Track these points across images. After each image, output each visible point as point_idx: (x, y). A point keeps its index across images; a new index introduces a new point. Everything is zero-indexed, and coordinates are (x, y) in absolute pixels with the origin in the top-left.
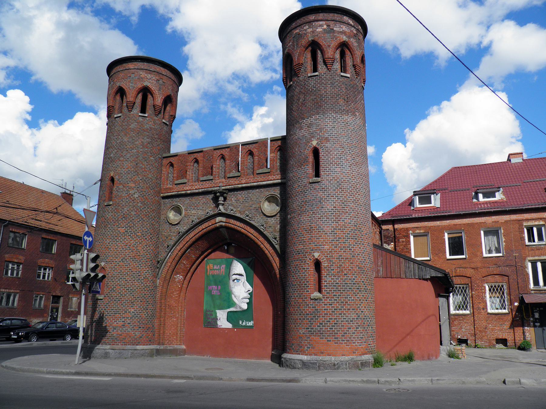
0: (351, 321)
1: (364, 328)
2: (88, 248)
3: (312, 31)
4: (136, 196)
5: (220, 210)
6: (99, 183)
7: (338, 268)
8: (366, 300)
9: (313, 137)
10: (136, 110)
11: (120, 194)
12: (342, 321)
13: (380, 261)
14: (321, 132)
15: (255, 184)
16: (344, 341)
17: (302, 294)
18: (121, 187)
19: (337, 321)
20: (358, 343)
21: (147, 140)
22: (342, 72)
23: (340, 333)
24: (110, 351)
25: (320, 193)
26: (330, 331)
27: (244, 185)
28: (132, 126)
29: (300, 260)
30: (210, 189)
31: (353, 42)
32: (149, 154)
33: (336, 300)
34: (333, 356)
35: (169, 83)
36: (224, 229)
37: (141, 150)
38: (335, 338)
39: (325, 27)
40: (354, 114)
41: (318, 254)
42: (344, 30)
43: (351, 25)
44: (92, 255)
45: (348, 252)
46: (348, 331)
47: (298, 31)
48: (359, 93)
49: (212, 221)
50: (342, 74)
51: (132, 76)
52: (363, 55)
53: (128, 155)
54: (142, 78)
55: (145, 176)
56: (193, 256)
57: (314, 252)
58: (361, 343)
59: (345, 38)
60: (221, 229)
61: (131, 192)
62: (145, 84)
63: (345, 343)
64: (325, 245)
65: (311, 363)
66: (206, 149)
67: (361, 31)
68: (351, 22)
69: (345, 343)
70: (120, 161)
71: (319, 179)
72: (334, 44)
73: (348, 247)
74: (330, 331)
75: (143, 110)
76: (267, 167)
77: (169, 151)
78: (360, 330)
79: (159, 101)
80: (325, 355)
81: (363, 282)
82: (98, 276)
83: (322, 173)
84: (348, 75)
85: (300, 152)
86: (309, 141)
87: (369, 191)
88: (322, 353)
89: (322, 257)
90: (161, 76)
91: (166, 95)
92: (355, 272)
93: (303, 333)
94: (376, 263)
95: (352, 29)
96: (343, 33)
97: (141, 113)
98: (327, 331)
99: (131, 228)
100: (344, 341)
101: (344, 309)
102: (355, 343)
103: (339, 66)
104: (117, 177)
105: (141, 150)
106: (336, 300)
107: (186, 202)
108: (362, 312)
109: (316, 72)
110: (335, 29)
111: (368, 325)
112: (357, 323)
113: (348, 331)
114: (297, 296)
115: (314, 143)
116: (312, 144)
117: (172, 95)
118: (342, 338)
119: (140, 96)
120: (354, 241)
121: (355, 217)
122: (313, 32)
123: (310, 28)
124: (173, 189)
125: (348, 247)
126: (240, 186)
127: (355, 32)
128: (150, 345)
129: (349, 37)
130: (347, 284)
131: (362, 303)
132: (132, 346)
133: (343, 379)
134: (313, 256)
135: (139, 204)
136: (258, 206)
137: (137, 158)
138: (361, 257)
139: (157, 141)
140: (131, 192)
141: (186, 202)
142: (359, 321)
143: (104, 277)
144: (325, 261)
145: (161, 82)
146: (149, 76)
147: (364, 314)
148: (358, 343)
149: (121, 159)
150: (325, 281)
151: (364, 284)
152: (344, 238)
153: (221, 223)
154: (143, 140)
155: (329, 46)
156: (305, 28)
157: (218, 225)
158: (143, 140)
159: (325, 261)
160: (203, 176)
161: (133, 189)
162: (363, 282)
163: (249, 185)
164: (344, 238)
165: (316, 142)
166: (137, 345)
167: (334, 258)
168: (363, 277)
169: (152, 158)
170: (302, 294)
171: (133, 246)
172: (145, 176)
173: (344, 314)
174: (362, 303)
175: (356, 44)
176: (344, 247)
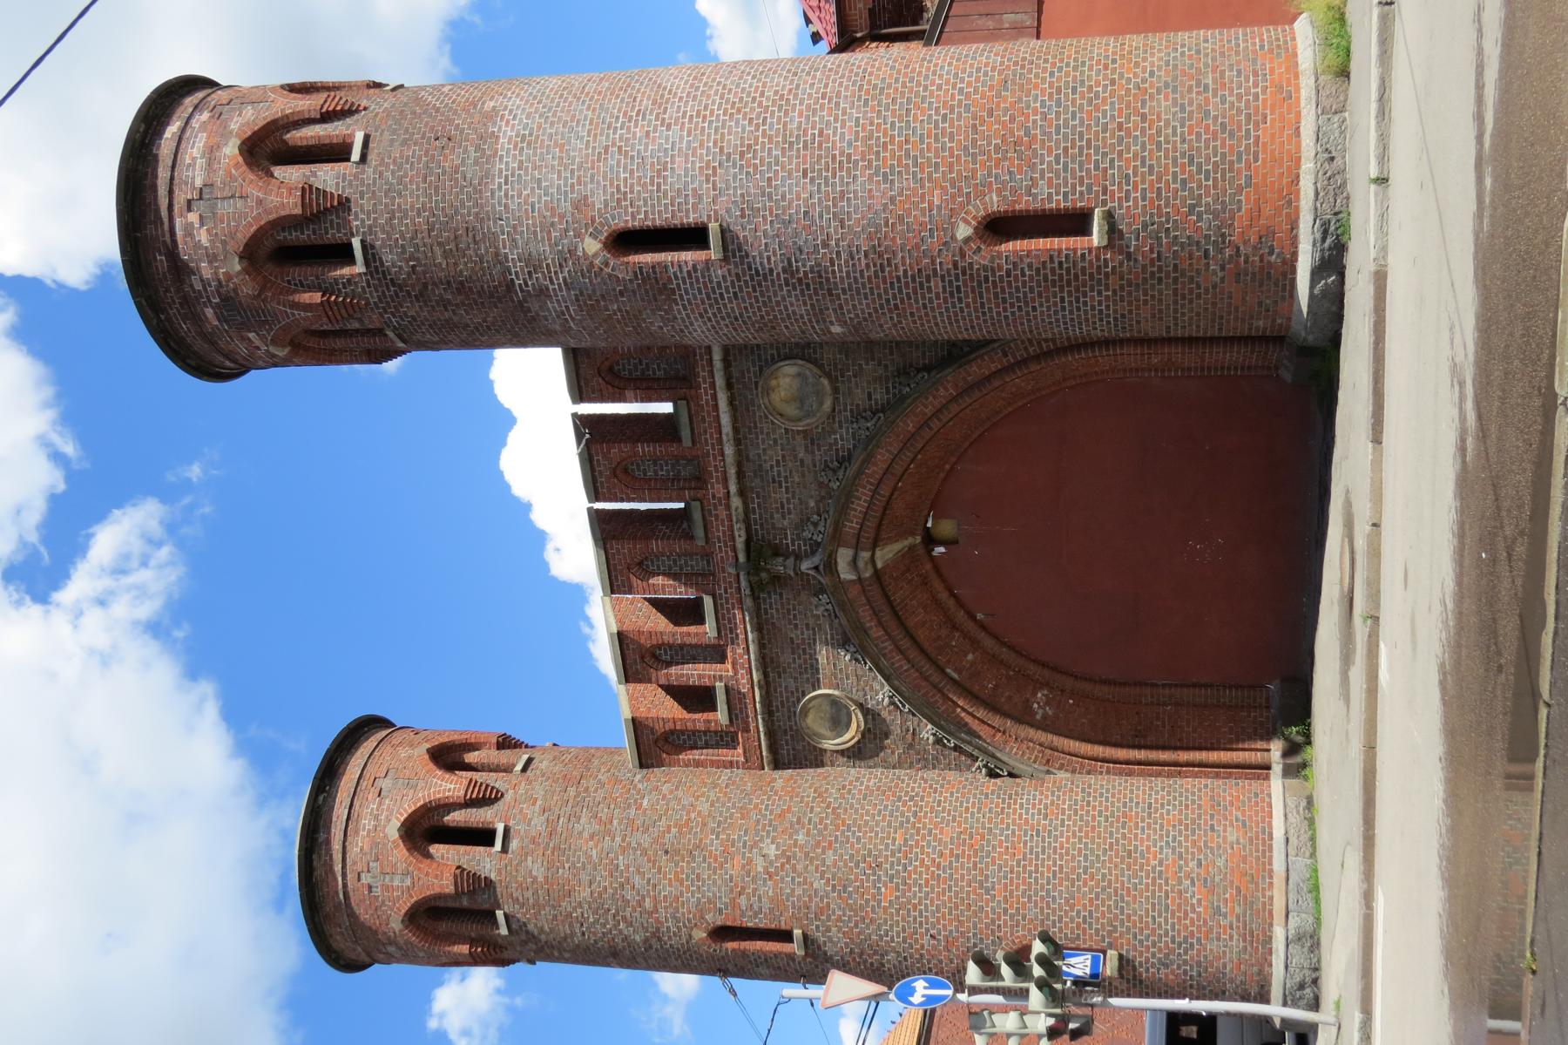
0: (1183, 109)
1: (1206, 65)
2: (950, 992)
3: (210, 262)
4: (772, 851)
5: (816, 568)
6: (733, 980)
7: (1005, 158)
8: (1114, 61)
10: (483, 860)
11: (766, 905)
12: (1183, 141)
13: (981, 22)
14: (553, 224)
16: (1248, 131)
17: (1091, 275)
18: (743, 901)
19: (1183, 155)
20: (1256, 85)
21: (583, 820)
22: (348, 160)
23: (1223, 145)
24: (1293, 923)
26: (1215, 179)
27: (733, 488)
28: (539, 872)
29: (980, 285)
31: (244, 121)
32: (633, 812)
33: (1112, 161)
34: (1298, 166)
35: (386, 757)
36: (878, 553)
37: (618, 839)
38: (1239, 161)
39: (193, 217)
40: (491, 116)
41: (962, 225)
42: (200, 154)
43: (183, 130)
44: (973, 974)
45: (951, 126)
46: (1216, 118)
47: (209, 312)
48: (418, 100)
50: (356, 156)
51: (366, 879)
52: (282, 87)
54: (375, 844)
55: (704, 825)
56: (970, 657)
58: (1256, 74)
59: (231, 149)
60: (879, 565)
61: (760, 865)
62: (393, 830)
63: (1257, 128)
64: (931, 203)
65: (1324, 239)
66: (612, 620)
67: (200, 95)
68: (172, 130)
69: (1257, 128)
71: (713, 227)
72: (251, 184)
73: (936, 127)
74: (1215, 179)
75: (483, 837)
76: (682, 515)
77: (618, 751)
78: (1215, 81)
79: (450, 786)
80: (1298, 191)
81: (1052, 74)
82: (1040, 978)
83: (691, 219)
85: (621, 293)
87: (750, 62)
88: (1290, 202)
90: (364, 784)
91: (431, 765)
92: (1020, 99)
94: (992, 36)
95: (195, 123)
96: (211, 152)
97: (491, 844)
98: (1215, 187)
100: (1248, 131)
102: (1256, 96)
103: (327, 167)
105: (618, 839)
106: (1112, 161)
107: (792, 684)
108: (1152, 74)
110: (198, 183)
111: (1198, 52)
112: (1190, 90)
113: (1216, 118)
114: (1100, 293)
115: (592, 246)
116: (595, 255)
117: (428, 746)
118: (1239, 140)
119: (437, 850)
120: (917, 107)
121: (837, 104)
122: (212, 259)
125: (936, 127)
127: (205, 116)
128: (1269, 796)
129: (226, 135)
130: (1058, 127)
131: (1121, 76)
132: (1275, 853)
133: (1373, 122)
134: (967, 240)
135: (801, 838)
136: (799, 438)
137: (644, 852)
138: (969, 85)
139: (587, 790)
140: (760, 865)
141: (792, 684)
142: (1183, 85)
143: (1046, 938)
144: (984, 204)
145: (385, 784)
146: (367, 823)
147: (1160, 68)
148: (1256, 85)
149: (648, 903)
150: (1050, 201)
151: (1060, 69)
152: (907, 142)
153: (861, 564)
154: (586, 835)
155: (260, 202)
158: (586, 835)
159: (984, 204)
160: (690, 537)
161: (750, 861)
162: (1052, 74)
163: (732, 471)
164: (907, 142)
165: (588, 240)
166: (1271, 838)
167: (974, 171)
168: (1037, 76)
169: (645, 803)
170: (1091, 275)
171: (941, 855)
172: (704, 825)
173: (1159, 133)
174: (1121, 76)
175: (249, 112)
176: (936, 140)
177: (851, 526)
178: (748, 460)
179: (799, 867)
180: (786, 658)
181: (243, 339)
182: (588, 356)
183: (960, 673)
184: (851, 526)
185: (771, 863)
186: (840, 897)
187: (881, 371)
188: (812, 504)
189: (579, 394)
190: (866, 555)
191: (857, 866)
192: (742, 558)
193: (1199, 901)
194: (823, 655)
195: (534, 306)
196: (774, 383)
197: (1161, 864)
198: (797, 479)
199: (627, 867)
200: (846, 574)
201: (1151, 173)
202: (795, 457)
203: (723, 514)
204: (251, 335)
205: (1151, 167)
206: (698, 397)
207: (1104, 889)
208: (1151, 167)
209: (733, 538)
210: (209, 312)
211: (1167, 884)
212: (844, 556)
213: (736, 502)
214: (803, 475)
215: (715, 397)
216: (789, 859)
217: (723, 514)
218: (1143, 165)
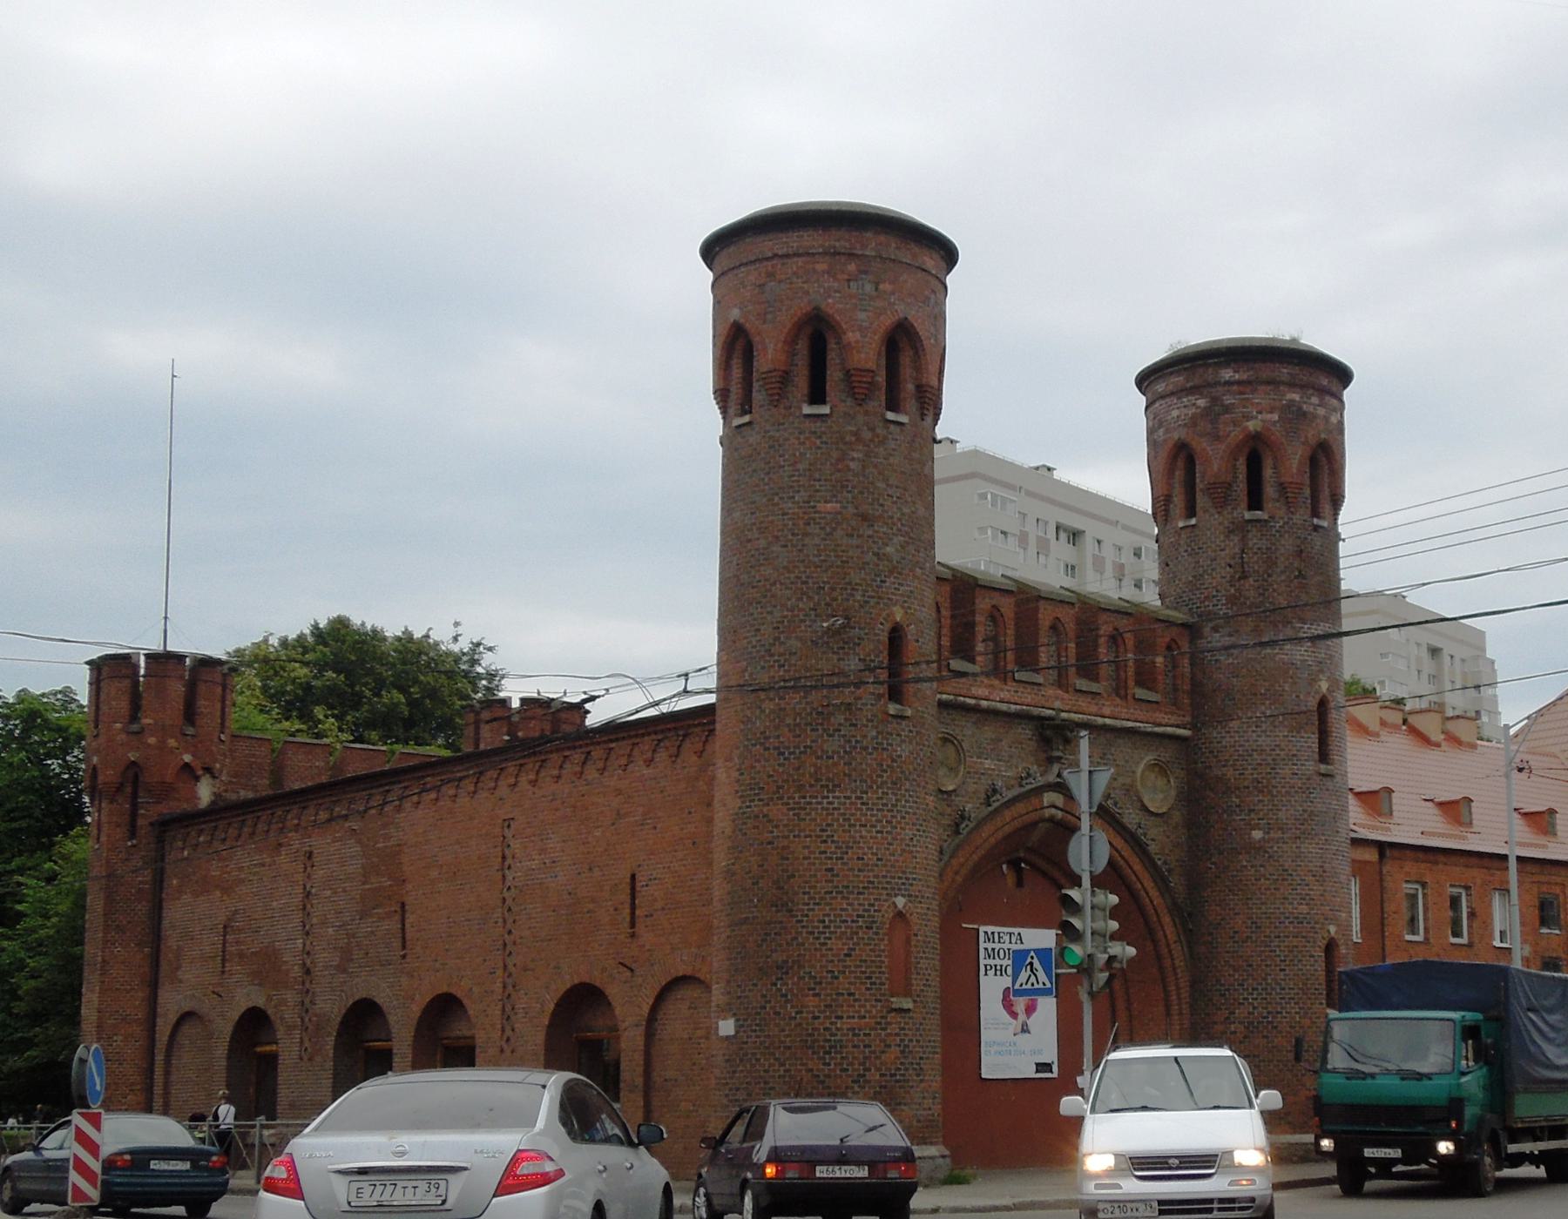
27: (1108, 721)
30: (1036, 711)
47: (1296, 397)
49: (1035, 801)
86: (1313, 681)
109: (823, 402)
126: (1100, 721)
153: (1053, 811)
157: (1048, 813)
210: (1296, 397)
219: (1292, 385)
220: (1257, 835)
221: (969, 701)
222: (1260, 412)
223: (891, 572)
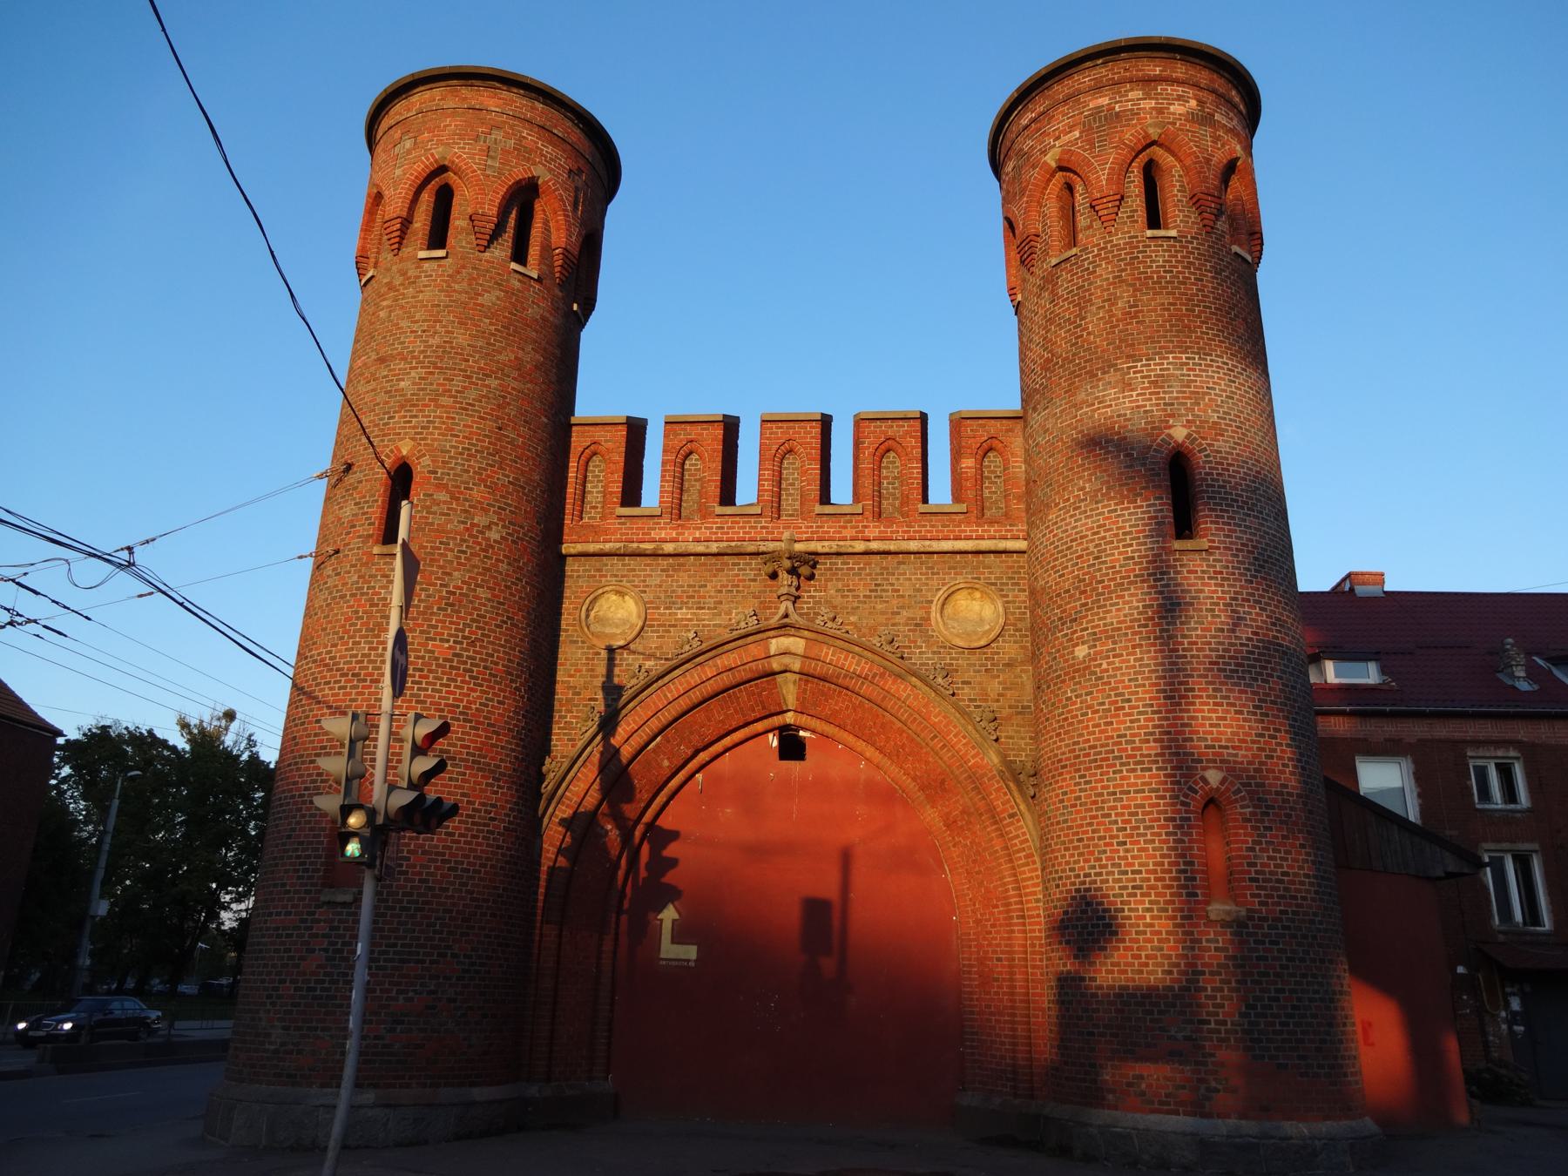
9: (1172, 416)
15: (913, 546)
19: (1299, 1000)
25: (1208, 585)
27: (874, 546)
39: (1193, 103)
47: (1105, 101)
49: (755, 650)
53: (472, 394)
57: (1205, 769)
70: (437, 406)
84: (1173, 233)
89: (1232, 783)
93: (1186, 1038)
99: (472, 644)
101: (1313, 960)
104: (426, 461)
122: (1160, 111)
123: (1147, 96)
124: (606, 532)
136: (922, 613)
153: (786, 660)
156: (1131, 95)
177: (828, 654)
178: (899, 563)
179: (476, 560)
180: (683, 579)
181: (1072, 128)
182: (1008, 431)
183: (654, 750)
184: (828, 654)
185: (482, 533)
186: (441, 598)
187: (993, 695)
188: (852, 619)
189: (959, 423)
190: (797, 666)
191: (473, 620)
192: (799, 547)
193: (411, 999)
194: (188, 748)
195: (1112, 376)
196: (977, 595)
197: (454, 956)
198: (879, 607)
199: (488, 386)
200: (776, 644)
201: (1282, 967)
202: (903, 607)
203: (848, 533)
204: (1077, 134)
205: (1287, 967)
206: (969, 523)
207: (430, 889)
208: (1287, 967)
209: (820, 540)
210: (1105, 101)
211: (432, 962)
212: (796, 644)
213: (860, 546)
214: (883, 613)
215: (969, 538)
216: (486, 551)
217: (848, 533)
218: (1289, 959)
219: (1098, 88)
220: (1081, 652)
221: (643, 546)
222: (1058, 138)
223: (402, 406)
